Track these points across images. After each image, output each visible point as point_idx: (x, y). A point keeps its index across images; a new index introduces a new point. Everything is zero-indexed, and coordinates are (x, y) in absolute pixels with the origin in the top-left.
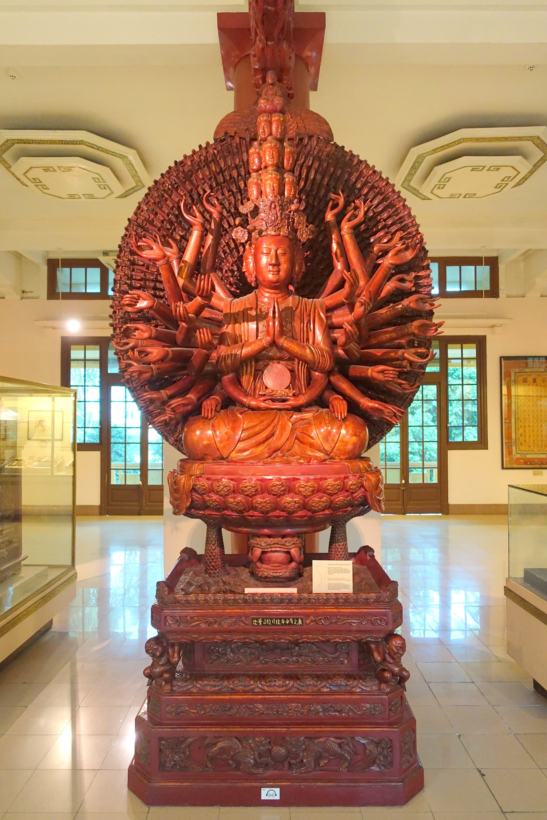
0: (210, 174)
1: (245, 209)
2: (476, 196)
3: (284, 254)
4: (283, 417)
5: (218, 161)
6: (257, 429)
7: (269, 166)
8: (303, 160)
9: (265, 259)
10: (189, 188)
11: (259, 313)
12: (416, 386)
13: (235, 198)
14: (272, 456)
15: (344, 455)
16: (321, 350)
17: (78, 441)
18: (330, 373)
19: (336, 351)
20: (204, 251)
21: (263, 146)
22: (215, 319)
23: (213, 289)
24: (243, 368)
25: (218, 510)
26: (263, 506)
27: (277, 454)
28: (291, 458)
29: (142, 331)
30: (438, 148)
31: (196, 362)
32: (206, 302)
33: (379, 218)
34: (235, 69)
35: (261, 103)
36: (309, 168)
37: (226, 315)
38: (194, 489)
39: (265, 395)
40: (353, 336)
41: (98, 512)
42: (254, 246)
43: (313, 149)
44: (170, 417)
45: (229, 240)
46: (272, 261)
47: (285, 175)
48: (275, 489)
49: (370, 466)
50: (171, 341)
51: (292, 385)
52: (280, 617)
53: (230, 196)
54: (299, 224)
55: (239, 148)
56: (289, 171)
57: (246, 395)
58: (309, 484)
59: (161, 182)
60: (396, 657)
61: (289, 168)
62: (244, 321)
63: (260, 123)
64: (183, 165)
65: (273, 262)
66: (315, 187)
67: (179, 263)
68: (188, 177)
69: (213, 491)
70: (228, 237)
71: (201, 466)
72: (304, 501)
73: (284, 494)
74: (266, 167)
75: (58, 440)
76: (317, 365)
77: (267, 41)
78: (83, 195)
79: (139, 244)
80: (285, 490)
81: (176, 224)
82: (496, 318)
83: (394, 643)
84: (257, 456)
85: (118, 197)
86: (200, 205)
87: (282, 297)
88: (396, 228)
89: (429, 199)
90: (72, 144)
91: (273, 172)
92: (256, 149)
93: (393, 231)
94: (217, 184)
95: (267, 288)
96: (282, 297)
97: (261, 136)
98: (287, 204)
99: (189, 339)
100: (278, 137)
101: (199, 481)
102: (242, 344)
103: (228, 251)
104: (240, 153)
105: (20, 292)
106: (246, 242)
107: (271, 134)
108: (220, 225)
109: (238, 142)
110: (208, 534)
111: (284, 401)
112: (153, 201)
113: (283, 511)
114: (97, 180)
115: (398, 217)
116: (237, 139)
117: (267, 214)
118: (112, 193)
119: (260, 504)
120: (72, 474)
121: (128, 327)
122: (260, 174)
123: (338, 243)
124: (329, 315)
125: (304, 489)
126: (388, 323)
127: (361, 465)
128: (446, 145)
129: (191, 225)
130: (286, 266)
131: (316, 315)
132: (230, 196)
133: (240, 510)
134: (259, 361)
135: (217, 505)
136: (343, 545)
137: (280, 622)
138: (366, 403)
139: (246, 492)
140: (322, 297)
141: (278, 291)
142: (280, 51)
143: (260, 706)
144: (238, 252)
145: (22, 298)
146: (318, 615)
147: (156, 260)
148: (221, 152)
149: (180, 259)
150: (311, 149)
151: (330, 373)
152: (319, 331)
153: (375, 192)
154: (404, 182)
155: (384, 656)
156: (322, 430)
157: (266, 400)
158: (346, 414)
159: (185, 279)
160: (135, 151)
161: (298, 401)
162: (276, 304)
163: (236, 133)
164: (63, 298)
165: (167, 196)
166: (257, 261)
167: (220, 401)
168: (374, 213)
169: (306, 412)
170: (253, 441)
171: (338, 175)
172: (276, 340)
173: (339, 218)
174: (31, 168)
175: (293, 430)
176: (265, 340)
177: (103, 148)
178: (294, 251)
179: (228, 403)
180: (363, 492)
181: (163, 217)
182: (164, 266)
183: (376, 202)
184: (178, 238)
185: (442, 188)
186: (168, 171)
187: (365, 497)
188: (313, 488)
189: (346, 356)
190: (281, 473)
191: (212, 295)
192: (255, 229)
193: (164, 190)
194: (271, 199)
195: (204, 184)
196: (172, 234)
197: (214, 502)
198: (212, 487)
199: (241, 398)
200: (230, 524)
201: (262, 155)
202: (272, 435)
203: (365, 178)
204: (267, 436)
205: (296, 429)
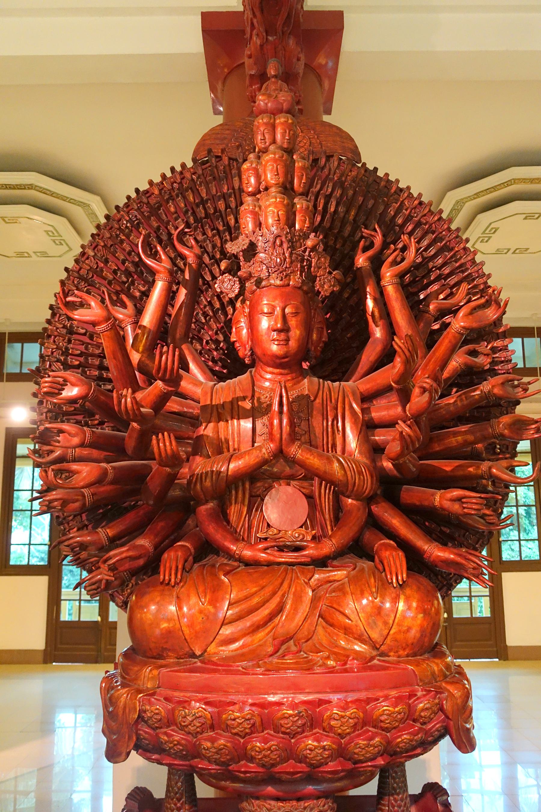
0: (186, 206)
1: (232, 248)
2: (528, 251)
3: (295, 314)
4: (298, 578)
5: (198, 190)
6: (256, 600)
7: (271, 187)
8: (319, 186)
9: (266, 323)
10: (155, 225)
11: (256, 405)
13: (221, 239)
14: (281, 652)
15: (404, 649)
16: (356, 462)
18: (370, 500)
19: (378, 464)
20: (173, 312)
21: (262, 159)
22: (188, 414)
23: (186, 368)
24: (230, 492)
25: (184, 758)
26: (265, 756)
27: (288, 648)
28: (312, 656)
29: (69, 434)
30: (482, 191)
31: (154, 484)
32: (170, 389)
33: (431, 264)
34: (224, 83)
35: (260, 100)
36: (328, 198)
37: (204, 408)
39: (266, 539)
40: (413, 442)
41: (40, 657)
42: (248, 303)
43: (332, 172)
45: (212, 297)
46: (276, 324)
47: (296, 200)
48: (287, 724)
50: (116, 449)
51: (311, 522)
53: (214, 235)
54: (319, 268)
55: (228, 171)
56: (302, 194)
57: (236, 540)
58: (348, 713)
59: (116, 219)
61: (301, 189)
62: (232, 418)
63: (258, 127)
64: (148, 195)
65: (279, 326)
66: (338, 224)
67: (134, 330)
68: (154, 211)
69: (176, 725)
70: (210, 293)
71: (155, 672)
72: (340, 744)
73: (303, 732)
74: (266, 189)
76: (350, 488)
77: (267, 35)
78: (34, 252)
79: (68, 299)
80: (304, 725)
81: (136, 277)
84: (253, 651)
86: (171, 248)
87: (293, 379)
88: (456, 280)
90: (18, 189)
91: (279, 195)
92: (252, 163)
93: (452, 283)
94: (196, 220)
95: (269, 366)
96: (293, 379)
97: (260, 145)
98: (299, 240)
99: (143, 449)
100: (285, 146)
101: (150, 703)
102: (229, 456)
103: (211, 313)
104: (228, 176)
106: (237, 297)
107: (274, 142)
108: (197, 274)
109: (227, 163)
110: (169, 779)
111: (297, 549)
112: (102, 244)
113: (300, 762)
114: (51, 234)
115: (457, 265)
116: (225, 160)
117: (268, 255)
118: (70, 249)
121: (47, 428)
122: (259, 199)
123: (375, 300)
124: (365, 406)
126: (460, 419)
128: (492, 188)
129: (153, 272)
130: (298, 332)
131: (347, 407)
132: (214, 235)
134: (256, 481)
135: (182, 750)
139: (234, 728)
140: (353, 378)
141: (286, 371)
142: (285, 50)
144: (226, 314)
147: (94, 324)
148: (202, 177)
149: (136, 323)
150: (329, 174)
151: (370, 500)
152: (352, 433)
153: (424, 229)
156: (365, 602)
157: (266, 548)
158: (405, 576)
159: (143, 352)
160: (98, 198)
161: (322, 549)
162: (283, 390)
163: (223, 151)
164: (8, 380)
165: (123, 238)
166: (253, 326)
167: (193, 551)
168: (424, 258)
169: (337, 568)
170: (247, 623)
171: (370, 206)
172: (283, 447)
173: (377, 263)
175: (315, 600)
176: (266, 448)
177: (58, 194)
178: (311, 310)
179: (206, 549)
180: (443, 721)
181: (117, 265)
182: (108, 333)
183: (425, 243)
184: (138, 294)
185: (487, 241)
186: (126, 204)
188: (356, 720)
189: (395, 472)
190: (297, 688)
191: (179, 378)
192: (250, 276)
193: (119, 229)
194: (275, 232)
195: (176, 219)
196: (129, 289)
198: (173, 715)
199: (227, 544)
201: (263, 171)
202: (280, 609)
203: (409, 211)
204: (270, 614)
205: (320, 598)
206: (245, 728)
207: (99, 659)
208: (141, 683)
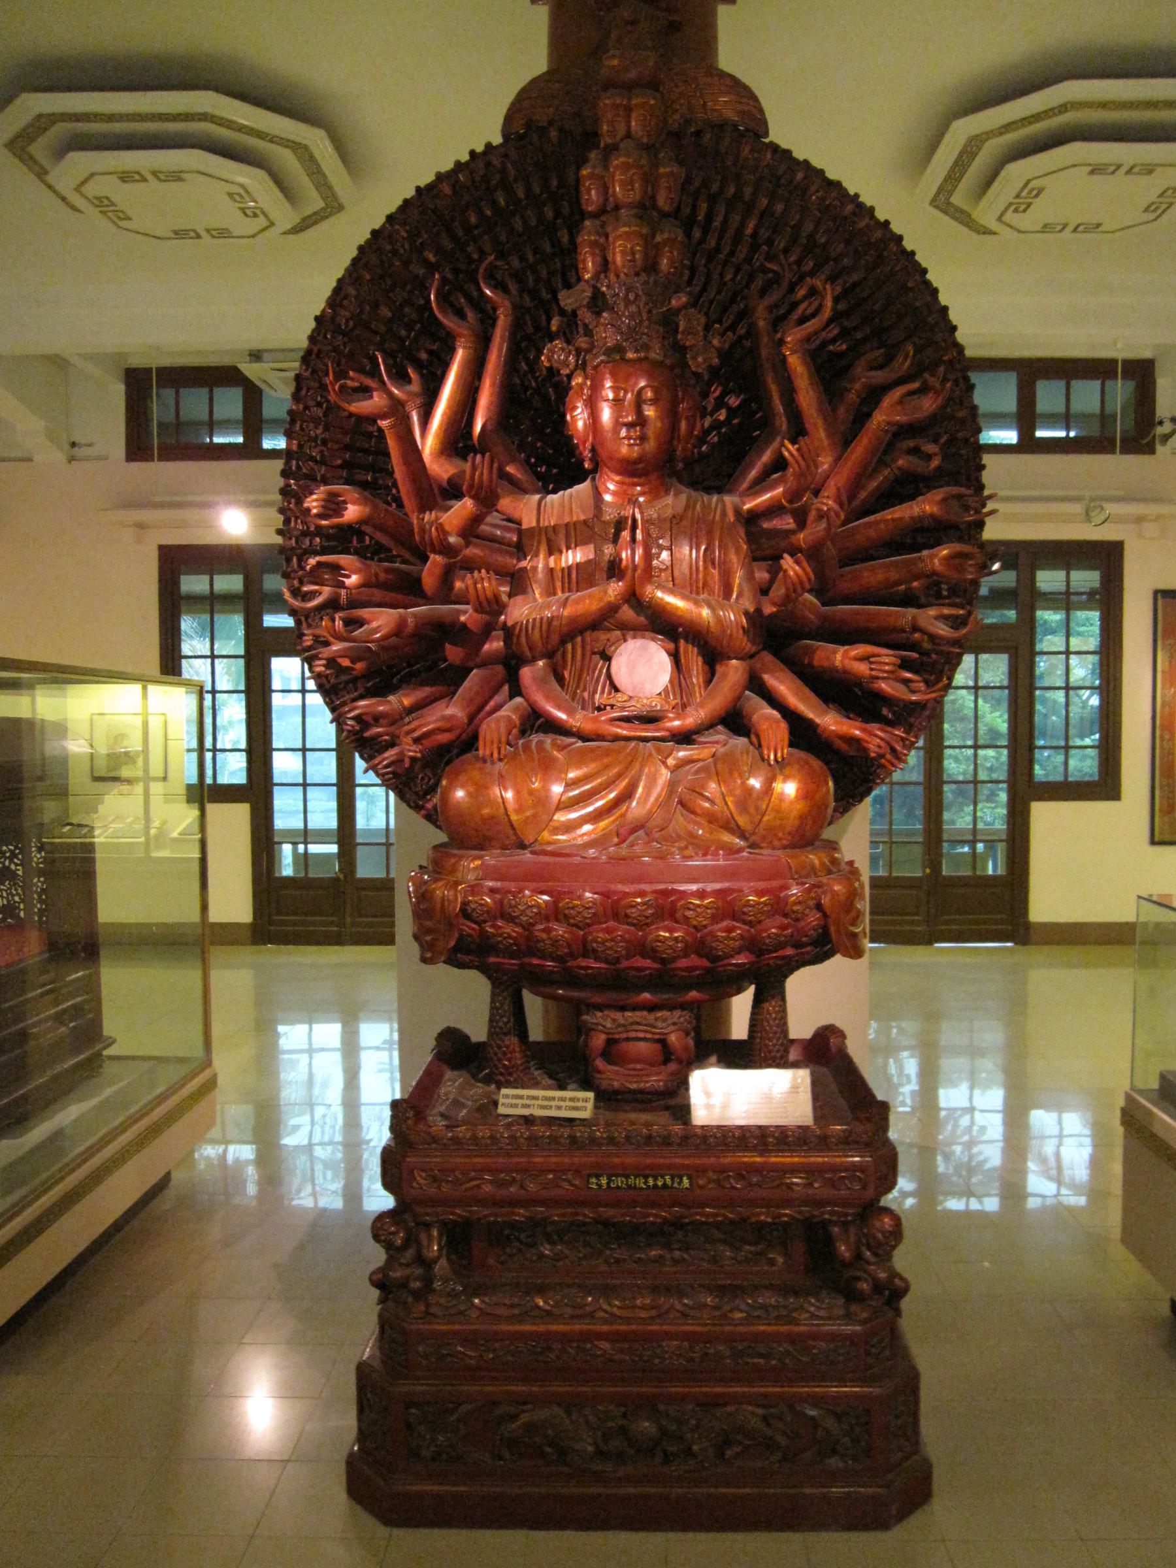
1: (567, 299)
12: (940, 685)
26: (610, 948)
38: (465, 913)
49: (834, 861)
60: (880, 1252)
62: (568, 548)
74: (617, 208)
75: (156, 779)
82: (1144, 500)
83: (877, 1224)
85: (285, 233)
89: (995, 233)
92: (594, 167)
105: (67, 446)
118: (272, 224)
127: (814, 858)
133: (562, 957)
135: (511, 945)
136: (778, 1026)
137: (645, 1183)
138: (830, 721)
143: (605, 1345)
145: (72, 459)
146: (722, 1170)
155: (858, 1248)
166: (594, 415)
167: (518, 722)
174: (92, 175)
175: (672, 785)
185: (1025, 211)
187: (825, 928)
188: (714, 911)
200: (540, 981)
201: (610, 181)
208: (460, 875)
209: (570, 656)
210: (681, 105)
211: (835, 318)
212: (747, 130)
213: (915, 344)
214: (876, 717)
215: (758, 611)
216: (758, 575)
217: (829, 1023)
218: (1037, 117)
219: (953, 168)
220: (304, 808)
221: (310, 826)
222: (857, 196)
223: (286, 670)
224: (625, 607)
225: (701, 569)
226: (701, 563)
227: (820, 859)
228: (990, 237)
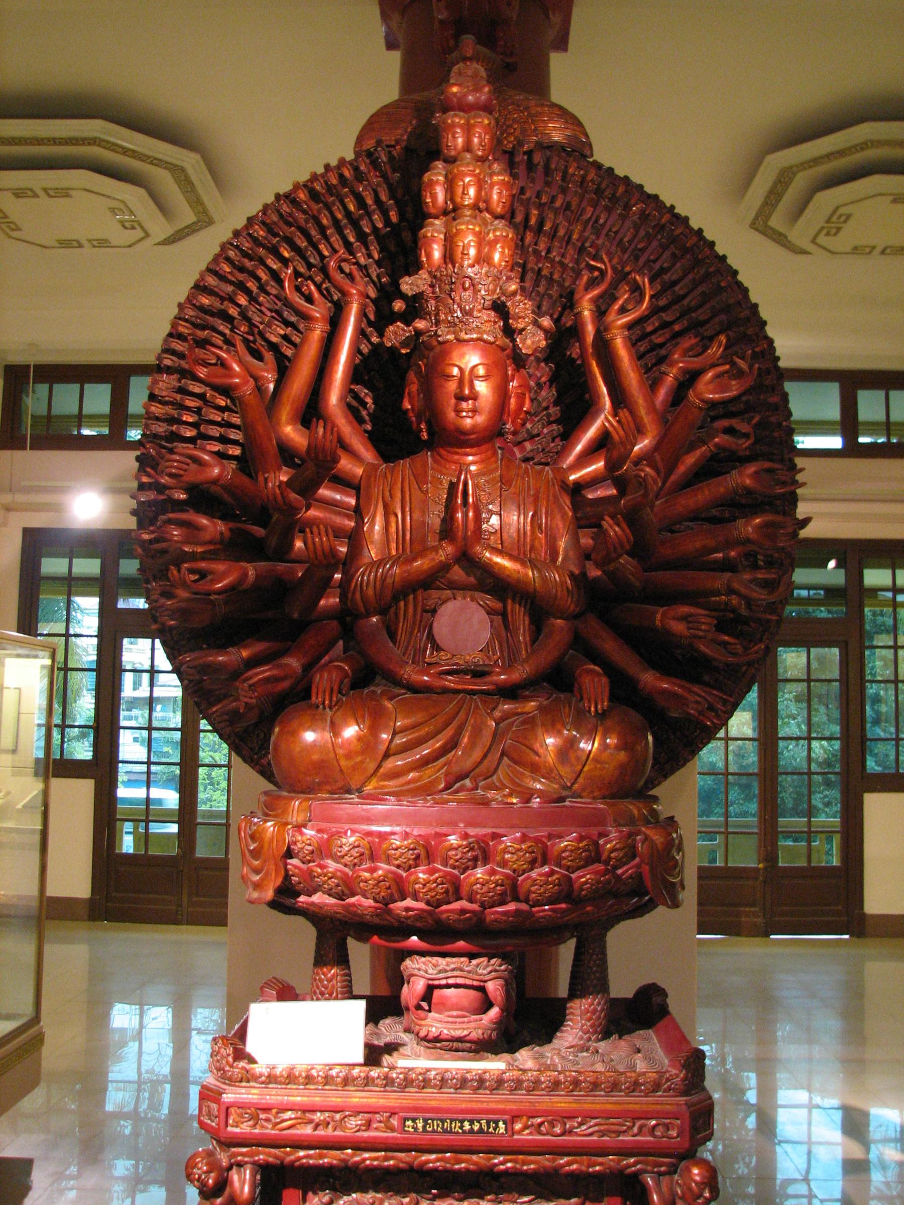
4: (477, 707)
17: (53, 757)
26: (431, 890)
44: (246, 703)
49: (654, 813)
52: (461, 1116)
85: (159, 244)
118: (147, 235)
119: (424, 885)
120: (39, 827)
125: (515, 857)
154: (756, 218)
175: (496, 736)
185: (835, 234)
197: (330, 878)
206: (409, 859)
207: (180, 917)
209: (402, 612)
210: (515, 129)
211: (655, 310)
212: (574, 151)
213: (728, 337)
214: (697, 680)
215: (584, 574)
216: (583, 541)
217: (650, 982)
218: (841, 153)
219: (768, 197)
220: (144, 783)
221: (54, 412)
222: (673, 207)
223: (138, 652)
224: (456, 568)
225: (529, 533)
226: (529, 528)
227: (639, 810)
228: (804, 257)
